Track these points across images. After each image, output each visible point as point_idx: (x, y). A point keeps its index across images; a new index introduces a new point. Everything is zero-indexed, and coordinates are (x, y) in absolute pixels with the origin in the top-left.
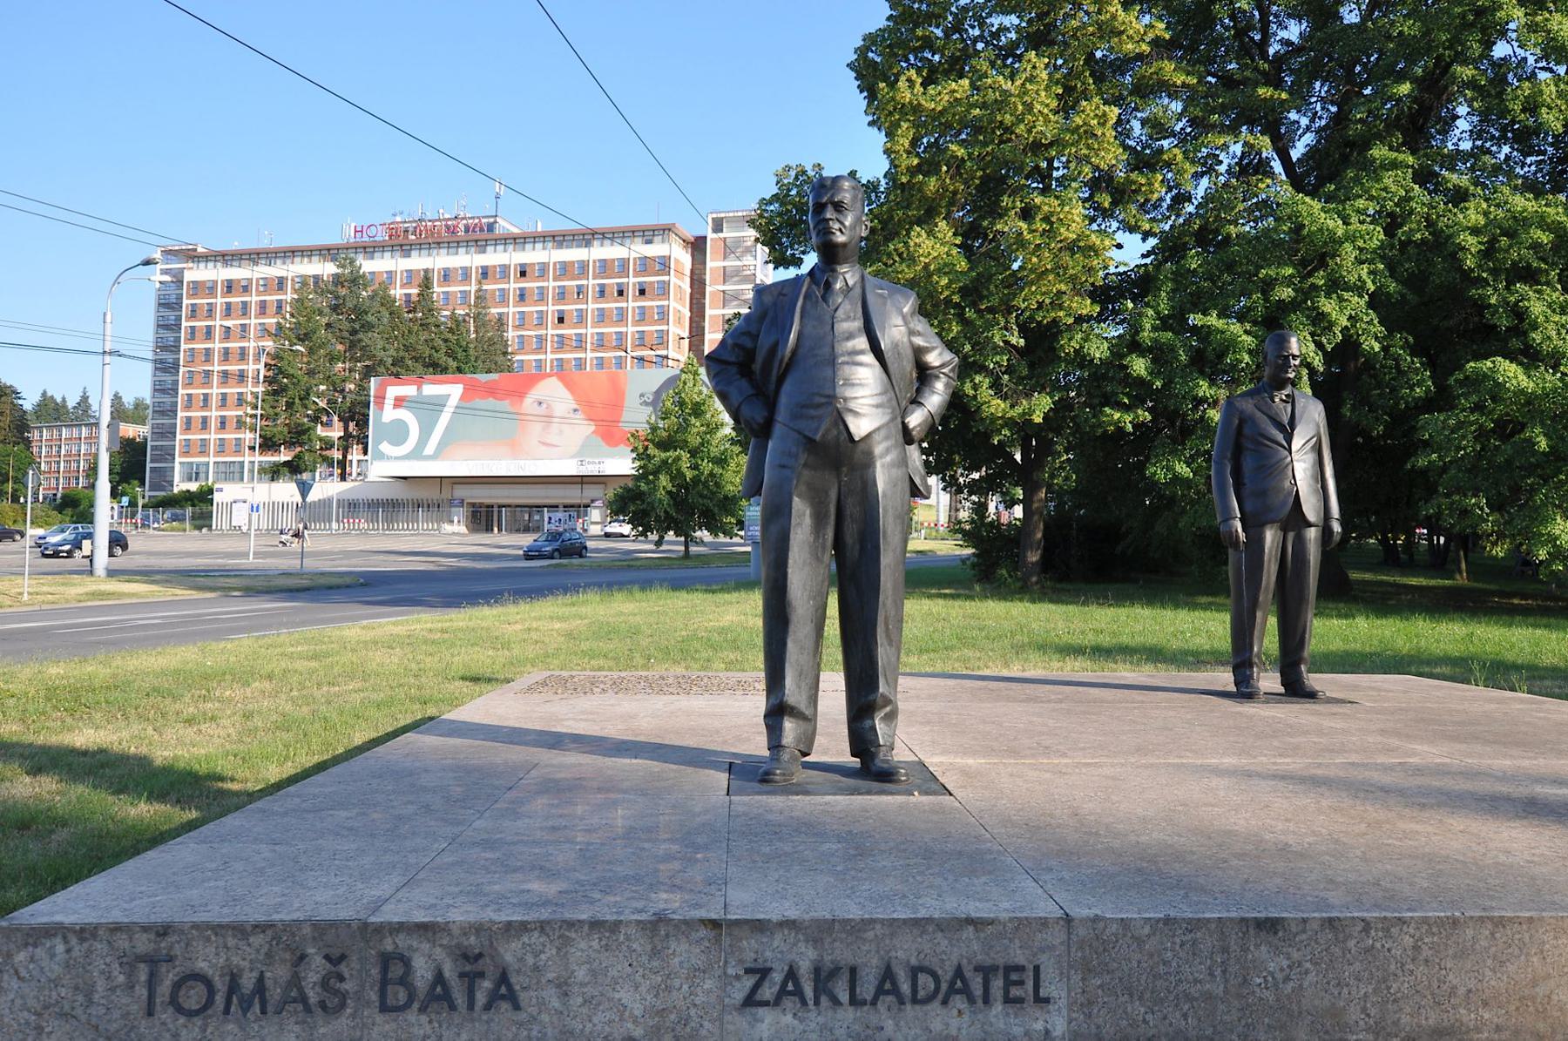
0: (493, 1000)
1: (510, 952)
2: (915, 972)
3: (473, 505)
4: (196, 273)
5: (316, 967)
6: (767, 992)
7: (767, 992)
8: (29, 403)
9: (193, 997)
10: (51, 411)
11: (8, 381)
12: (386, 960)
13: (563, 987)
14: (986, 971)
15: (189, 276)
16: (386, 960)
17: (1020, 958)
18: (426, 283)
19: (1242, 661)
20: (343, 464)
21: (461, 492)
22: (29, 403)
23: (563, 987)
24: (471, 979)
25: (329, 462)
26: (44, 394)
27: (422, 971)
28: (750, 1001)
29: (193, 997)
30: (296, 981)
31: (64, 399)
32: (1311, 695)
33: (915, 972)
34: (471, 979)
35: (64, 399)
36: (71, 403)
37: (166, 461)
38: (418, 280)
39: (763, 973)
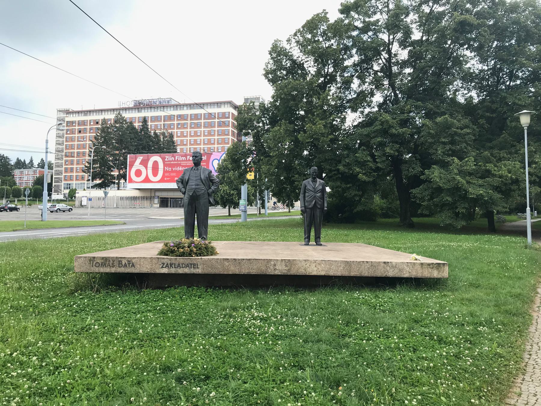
0: (132, 266)
1: (134, 261)
2: (182, 264)
3: (161, 198)
4: (70, 118)
5: (111, 262)
6: (164, 266)
7: (164, 266)
8: (12, 163)
9: (97, 265)
10: (20, 164)
11: (2, 153)
12: (119, 261)
13: (140, 265)
14: (191, 264)
15: (67, 119)
16: (119, 261)
17: (195, 263)
18: (145, 121)
19: (308, 238)
20: (118, 184)
21: (158, 194)
22: (12, 163)
23: (140, 265)
24: (129, 264)
25: (114, 183)
26: (18, 158)
27: (123, 263)
28: (162, 267)
29: (97, 265)
30: (109, 264)
31: (24, 161)
32: (321, 245)
33: (182, 264)
34: (129, 264)
35: (24, 161)
36: (27, 162)
37: (59, 182)
38: (141, 120)
39: (164, 264)
